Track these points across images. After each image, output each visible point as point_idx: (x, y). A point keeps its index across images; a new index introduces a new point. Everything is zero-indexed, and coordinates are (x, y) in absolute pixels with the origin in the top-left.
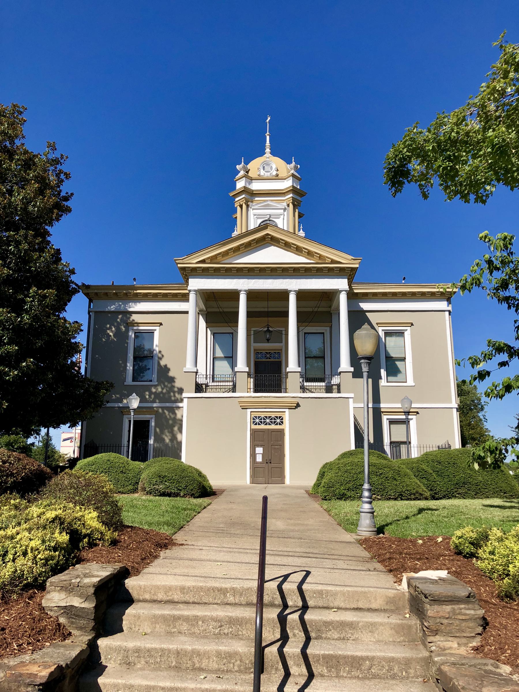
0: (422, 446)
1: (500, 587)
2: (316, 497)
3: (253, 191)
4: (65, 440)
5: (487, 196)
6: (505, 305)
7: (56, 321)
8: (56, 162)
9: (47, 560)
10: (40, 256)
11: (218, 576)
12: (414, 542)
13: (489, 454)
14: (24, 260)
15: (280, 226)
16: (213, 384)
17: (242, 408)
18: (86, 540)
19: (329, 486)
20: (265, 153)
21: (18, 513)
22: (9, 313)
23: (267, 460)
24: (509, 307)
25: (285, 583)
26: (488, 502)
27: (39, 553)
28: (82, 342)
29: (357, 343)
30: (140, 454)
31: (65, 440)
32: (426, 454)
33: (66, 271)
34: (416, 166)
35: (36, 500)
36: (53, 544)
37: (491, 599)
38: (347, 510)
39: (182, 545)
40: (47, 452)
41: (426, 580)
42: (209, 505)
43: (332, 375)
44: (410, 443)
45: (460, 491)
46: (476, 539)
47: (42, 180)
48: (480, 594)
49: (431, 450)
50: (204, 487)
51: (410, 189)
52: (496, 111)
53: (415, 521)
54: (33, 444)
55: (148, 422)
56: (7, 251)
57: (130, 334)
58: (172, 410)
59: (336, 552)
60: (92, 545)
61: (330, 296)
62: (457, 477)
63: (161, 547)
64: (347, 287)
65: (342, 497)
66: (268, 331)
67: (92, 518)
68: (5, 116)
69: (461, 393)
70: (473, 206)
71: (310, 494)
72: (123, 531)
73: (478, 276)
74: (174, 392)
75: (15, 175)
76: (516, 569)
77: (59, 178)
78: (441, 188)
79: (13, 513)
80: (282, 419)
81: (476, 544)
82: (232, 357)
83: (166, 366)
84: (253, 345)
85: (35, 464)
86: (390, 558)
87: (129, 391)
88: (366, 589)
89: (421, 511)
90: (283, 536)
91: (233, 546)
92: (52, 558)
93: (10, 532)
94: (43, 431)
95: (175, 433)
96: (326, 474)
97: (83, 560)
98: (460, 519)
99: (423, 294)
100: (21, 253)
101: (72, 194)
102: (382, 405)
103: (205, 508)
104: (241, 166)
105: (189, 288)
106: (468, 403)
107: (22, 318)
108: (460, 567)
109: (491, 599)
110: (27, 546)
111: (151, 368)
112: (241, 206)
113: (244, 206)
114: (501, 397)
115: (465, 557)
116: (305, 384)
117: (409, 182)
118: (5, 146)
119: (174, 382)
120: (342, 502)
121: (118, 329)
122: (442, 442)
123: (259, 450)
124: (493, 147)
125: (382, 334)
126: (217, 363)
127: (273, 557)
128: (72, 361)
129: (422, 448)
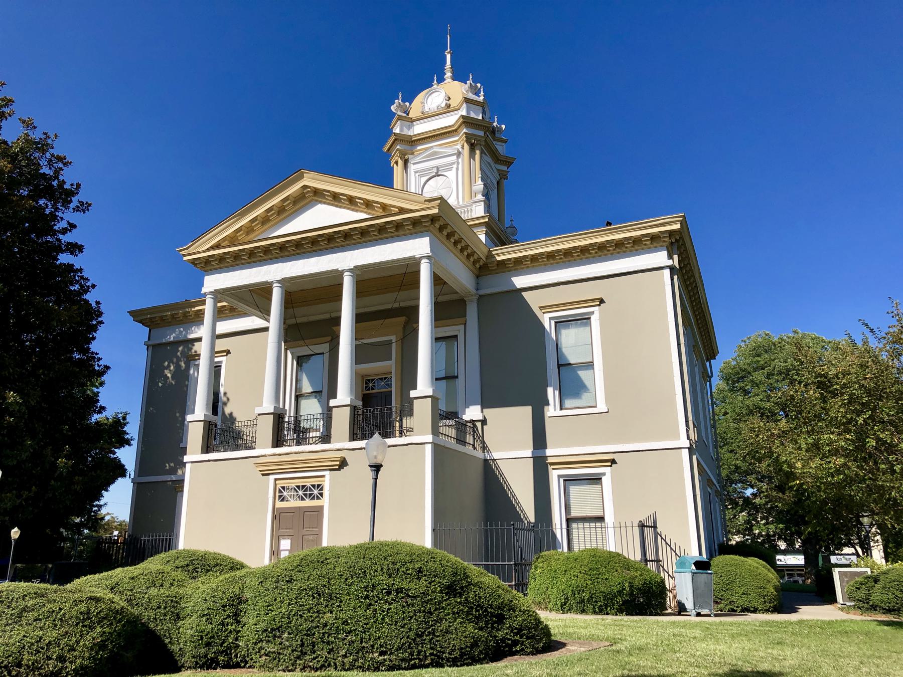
0: (623, 525)
3: (411, 137)
17: (263, 475)
83: (231, 414)
121: (178, 366)
126: (304, 403)
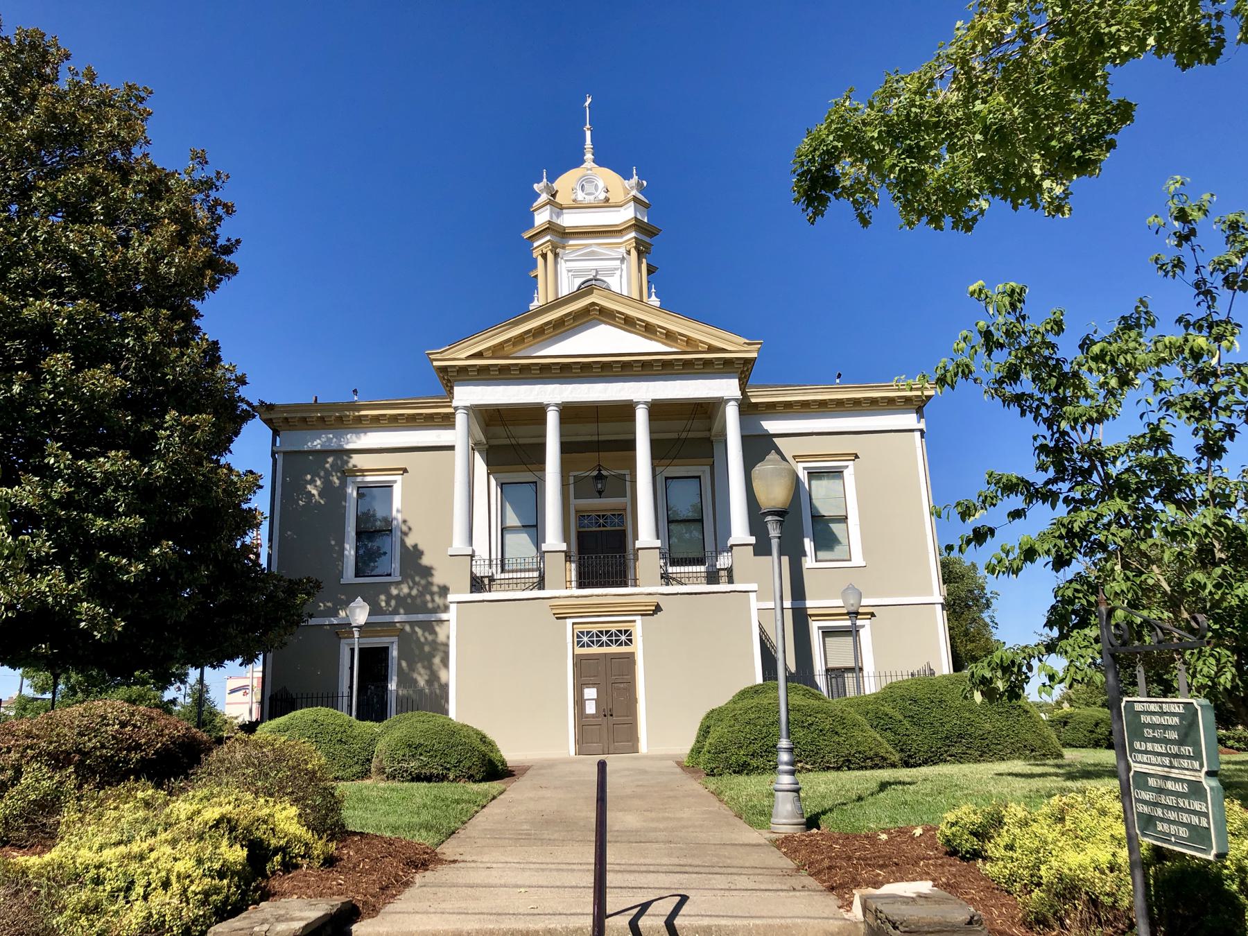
1: (1025, 905)
2: (696, 772)
3: (565, 228)
4: (233, 691)
5: (975, 219)
6: (1015, 410)
7: (213, 471)
8: (208, 185)
9: (206, 894)
10: (183, 354)
11: (521, 911)
12: (872, 838)
13: (999, 674)
14: (153, 362)
15: (615, 287)
16: (503, 576)
18: (278, 858)
19: (718, 752)
20: (583, 162)
21: (151, 814)
22: (128, 458)
23: (606, 711)
24: (1023, 413)
25: (643, 918)
26: (1003, 767)
27: (192, 882)
28: (260, 509)
29: (756, 485)
30: (373, 705)
31: (233, 691)
32: (891, 687)
33: (230, 380)
34: (848, 169)
35: (183, 790)
36: (217, 866)
37: (1010, 928)
38: (752, 790)
39: (454, 861)
40: (200, 714)
41: (894, 898)
42: (501, 793)
43: (717, 552)
44: (861, 669)
45: (953, 750)
46: (981, 825)
47: (183, 219)
48: (992, 921)
49: (900, 678)
50: (491, 762)
51: (839, 208)
52: (985, 71)
53: (874, 804)
54: (173, 701)
55: (385, 651)
56: (122, 346)
57: (349, 490)
58: (429, 627)
59: (735, 863)
60: (289, 866)
61: (708, 410)
62: (947, 727)
63: (416, 867)
64: (738, 394)
65: (743, 769)
66: (600, 477)
67: (288, 818)
68: (112, 106)
69: (949, 575)
70: (948, 232)
71: (685, 768)
72: (345, 840)
73: (967, 360)
74: (432, 594)
75: (134, 211)
76: (1053, 872)
77: (213, 213)
78: (896, 204)
79: (141, 814)
80: (630, 635)
81: (981, 834)
82: (536, 526)
83: (415, 546)
84: (574, 502)
85: (179, 727)
86: (830, 868)
87: (351, 593)
88: (789, 921)
89: (884, 786)
90: (637, 838)
91: (548, 860)
92: (217, 890)
93: (135, 848)
94: (193, 674)
95: (435, 667)
96: (712, 730)
97: (274, 895)
98: (950, 792)
99: (874, 401)
100: (147, 349)
101: (238, 242)
102: (809, 603)
103: (494, 798)
104: (542, 185)
105: (455, 404)
106: (963, 594)
107: (151, 467)
108: (954, 876)
109: (1010, 928)
110: (169, 871)
111: (389, 552)
112: (544, 256)
113: (550, 256)
114: (1016, 571)
115: (963, 858)
116: (670, 570)
117: (837, 197)
118: (115, 160)
119: (432, 575)
120: (742, 779)
122: (917, 666)
123: (590, 693)
124: (985, 131)
125: (803, 475)
126: (508, 537)
127: (619, 876)
128: (243, 544)
129: (883, 678)
